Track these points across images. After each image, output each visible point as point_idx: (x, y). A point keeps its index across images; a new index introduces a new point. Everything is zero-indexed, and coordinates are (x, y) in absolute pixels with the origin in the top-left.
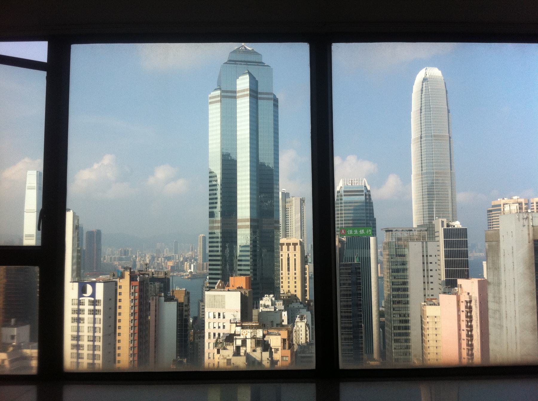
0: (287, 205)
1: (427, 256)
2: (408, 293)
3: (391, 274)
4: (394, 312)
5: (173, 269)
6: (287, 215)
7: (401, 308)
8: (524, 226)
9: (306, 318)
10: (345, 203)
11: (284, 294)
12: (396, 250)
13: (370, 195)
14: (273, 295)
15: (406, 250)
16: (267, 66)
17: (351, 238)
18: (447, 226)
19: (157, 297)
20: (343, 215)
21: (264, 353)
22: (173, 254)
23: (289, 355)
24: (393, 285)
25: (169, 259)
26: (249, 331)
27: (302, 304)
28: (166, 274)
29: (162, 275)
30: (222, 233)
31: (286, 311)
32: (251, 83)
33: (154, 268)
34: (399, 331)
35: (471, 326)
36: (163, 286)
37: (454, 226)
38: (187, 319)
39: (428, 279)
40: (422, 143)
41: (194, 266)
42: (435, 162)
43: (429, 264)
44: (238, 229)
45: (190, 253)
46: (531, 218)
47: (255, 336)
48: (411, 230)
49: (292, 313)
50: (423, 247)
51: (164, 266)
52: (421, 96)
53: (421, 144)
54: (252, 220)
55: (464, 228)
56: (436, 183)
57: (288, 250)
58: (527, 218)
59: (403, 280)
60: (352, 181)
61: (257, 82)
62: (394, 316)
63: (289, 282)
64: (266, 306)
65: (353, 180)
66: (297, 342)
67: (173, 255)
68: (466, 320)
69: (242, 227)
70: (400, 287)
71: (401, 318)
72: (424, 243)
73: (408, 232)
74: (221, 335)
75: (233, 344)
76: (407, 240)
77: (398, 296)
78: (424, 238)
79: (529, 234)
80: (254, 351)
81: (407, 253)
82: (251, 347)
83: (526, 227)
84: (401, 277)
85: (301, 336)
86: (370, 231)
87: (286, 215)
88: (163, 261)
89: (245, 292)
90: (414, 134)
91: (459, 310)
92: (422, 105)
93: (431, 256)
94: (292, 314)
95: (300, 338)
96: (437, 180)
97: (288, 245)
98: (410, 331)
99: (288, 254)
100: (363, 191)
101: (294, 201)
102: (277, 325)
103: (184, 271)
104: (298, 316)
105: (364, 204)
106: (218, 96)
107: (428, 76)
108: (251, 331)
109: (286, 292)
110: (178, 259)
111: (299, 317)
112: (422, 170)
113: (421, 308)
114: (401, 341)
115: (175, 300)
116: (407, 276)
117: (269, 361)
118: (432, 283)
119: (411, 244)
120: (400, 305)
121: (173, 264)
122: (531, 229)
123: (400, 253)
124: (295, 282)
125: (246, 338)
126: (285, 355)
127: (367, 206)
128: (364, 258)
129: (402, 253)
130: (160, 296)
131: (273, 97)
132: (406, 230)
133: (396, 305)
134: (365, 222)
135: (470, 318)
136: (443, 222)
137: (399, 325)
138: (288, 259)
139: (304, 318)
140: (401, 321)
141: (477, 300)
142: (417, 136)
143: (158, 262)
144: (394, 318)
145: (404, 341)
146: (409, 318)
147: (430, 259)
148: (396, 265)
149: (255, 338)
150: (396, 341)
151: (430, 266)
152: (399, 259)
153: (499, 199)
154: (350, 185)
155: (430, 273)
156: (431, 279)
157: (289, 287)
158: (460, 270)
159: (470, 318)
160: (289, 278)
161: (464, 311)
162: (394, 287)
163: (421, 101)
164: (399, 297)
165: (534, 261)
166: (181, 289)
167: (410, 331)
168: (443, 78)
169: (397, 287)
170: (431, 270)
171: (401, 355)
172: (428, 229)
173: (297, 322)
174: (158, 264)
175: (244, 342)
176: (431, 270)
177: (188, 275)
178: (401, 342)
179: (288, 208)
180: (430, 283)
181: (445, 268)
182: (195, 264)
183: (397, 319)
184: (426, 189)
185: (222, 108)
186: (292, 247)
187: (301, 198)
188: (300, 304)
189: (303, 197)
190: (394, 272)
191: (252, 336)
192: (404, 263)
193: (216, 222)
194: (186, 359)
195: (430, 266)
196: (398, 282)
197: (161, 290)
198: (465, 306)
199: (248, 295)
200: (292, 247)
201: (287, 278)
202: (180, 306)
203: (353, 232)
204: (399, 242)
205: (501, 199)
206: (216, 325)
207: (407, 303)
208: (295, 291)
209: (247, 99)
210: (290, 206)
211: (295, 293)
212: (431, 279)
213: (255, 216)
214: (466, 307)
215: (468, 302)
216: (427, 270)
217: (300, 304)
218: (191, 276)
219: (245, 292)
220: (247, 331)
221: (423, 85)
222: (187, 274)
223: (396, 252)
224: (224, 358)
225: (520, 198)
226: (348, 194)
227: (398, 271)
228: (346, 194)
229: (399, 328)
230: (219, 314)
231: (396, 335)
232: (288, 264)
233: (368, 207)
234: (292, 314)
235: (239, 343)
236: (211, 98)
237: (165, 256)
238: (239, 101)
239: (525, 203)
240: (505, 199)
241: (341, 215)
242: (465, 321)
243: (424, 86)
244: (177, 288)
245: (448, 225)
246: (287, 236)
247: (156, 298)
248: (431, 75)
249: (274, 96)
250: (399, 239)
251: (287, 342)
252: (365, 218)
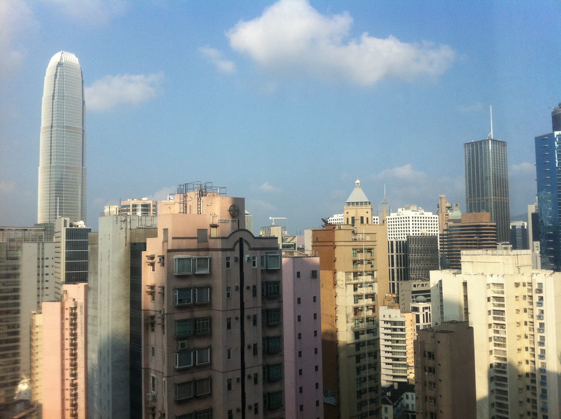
2: (19, 301)
7: (10, 318)
8: (122, 229)
12: (7, 253)
15: (19, 252)
18: (70, 226)
37: (78, 226)
40: (53, 132)
42: (66, 155)
43: (45, 268)
46: (129, 221)
50: (39, 249)
53: (51, 134)
55: (88, 229)
59: (14, 287)
70: (9, 294)
72: (41, 244)
73: (23, 232)
78: (41, 237)
79: (126, 237)
81: (20, 256)
83: (124, 230)
84: (12, 284)
90: (45, 122)
91: (62, 318)
92: (55, 91)
93: (47, 259)
96: (67, 175)
107: (63, 61)
112: (51, 163)
116: (18, 281)
122: (129, 232)
123: (11, 256)
129: (13, 256)
132: (21, 229)
135: (74, 325)
136: (65, 221)
140: (10, 334)
141: (82, 306)
142: (47, 125)
147: (46, 262)
151: (46, 270)
153: (128, 200)
159: (74, 325)
163: (54, 87)
165: (130, 265)
168: (79, 66)
170: (47, 274)
176: (47, 274)
192: (17, 267)
195: (46, 270)
196: (8, 289)
207: (18, 312)
214: (71, 314)
221: (57, 69)
223: (7, 255)
225: (149, 199)
240: (135, 199)
243: (59, 71)
245: (71, 225)
248: (67, 60)
250: (11, 240)
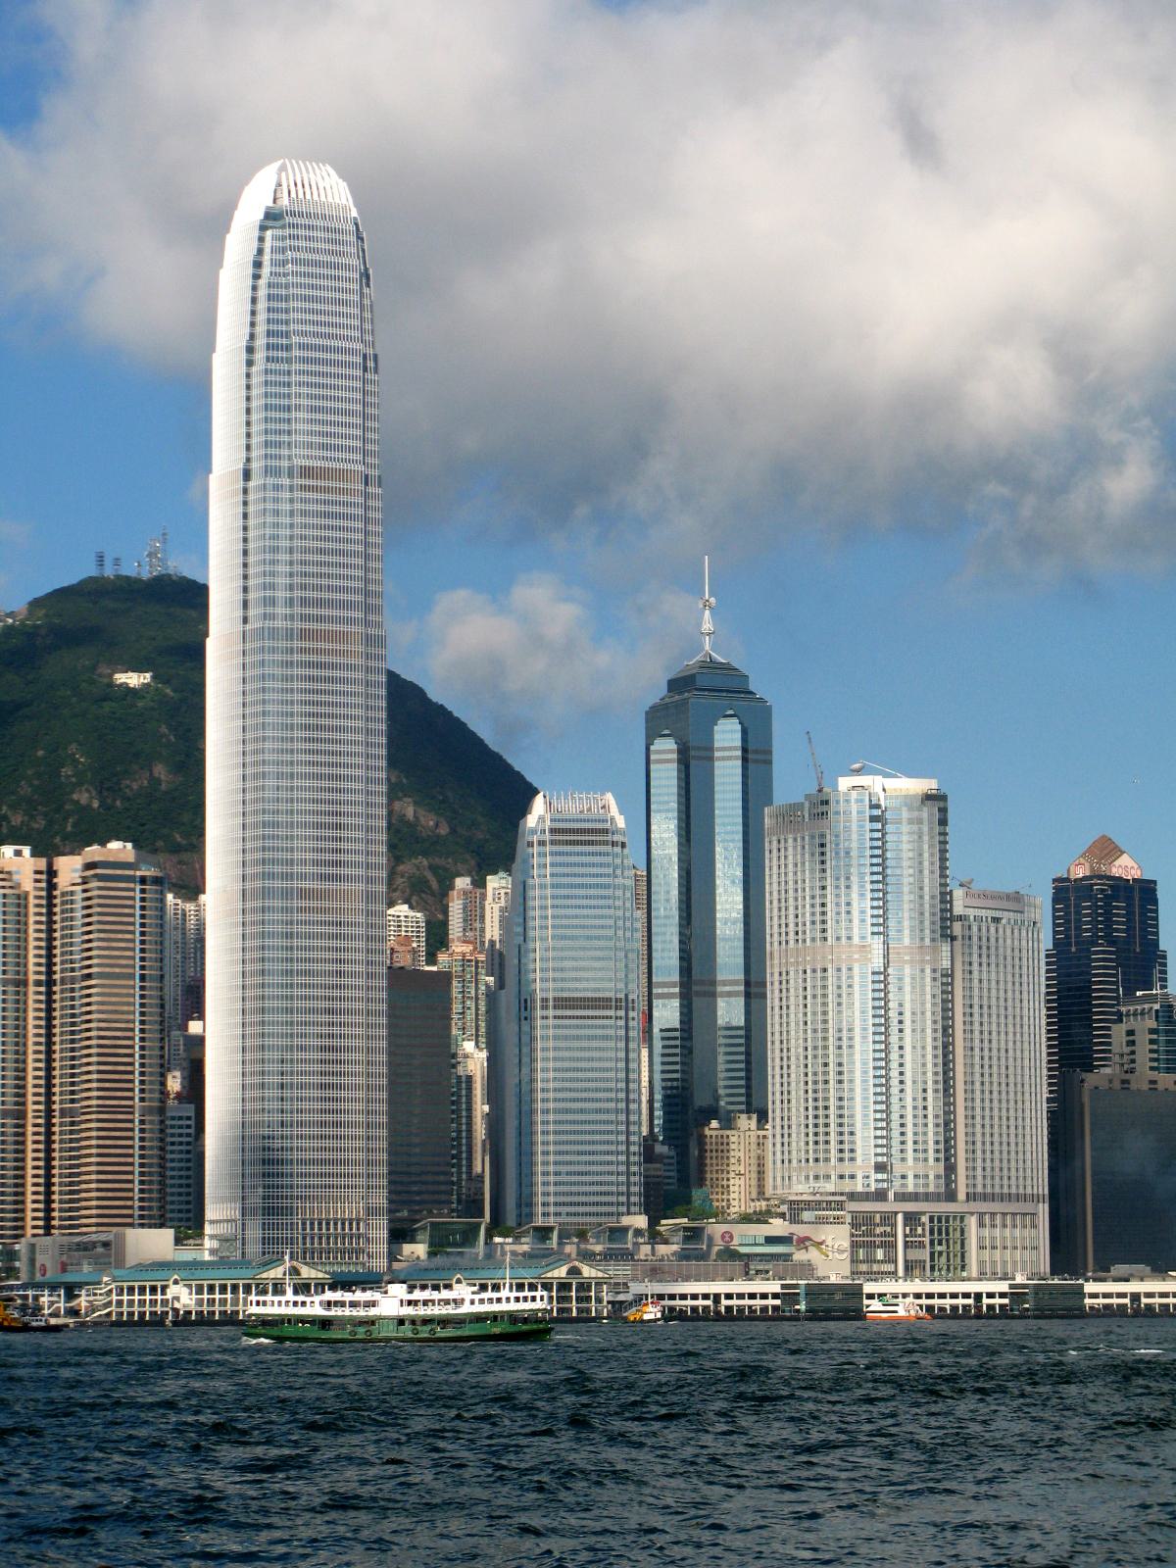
112: (245, 620)
221: (261, 239)
241: (543, 892)
243: (268, 245)
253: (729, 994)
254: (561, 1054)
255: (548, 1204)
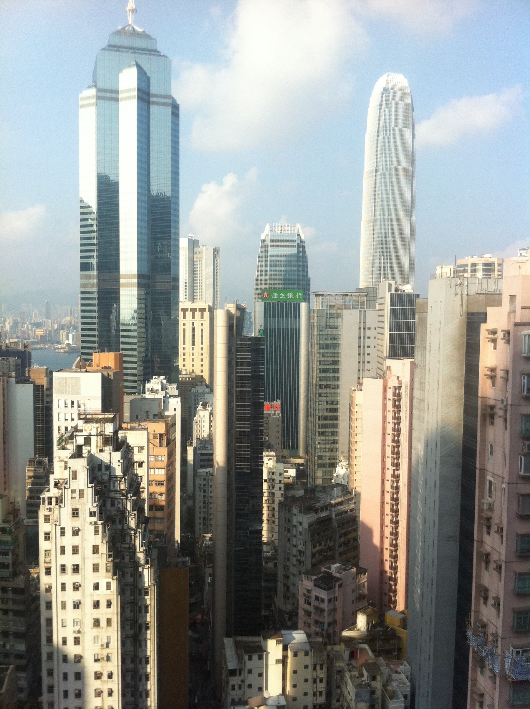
0: (196, 256)
1: (364, 328)
2: (339, 375)
3: (318, 351)
4: (320, 398)
5: (43, 340)
6: (195, 271)
9: (211, 406)
10: (271, 256)
11: (186, 374)
12: (326, 321)
13: (304, 247)
14: (164, 377)
15: (340, 320)
16: (164, 56)
17: (275, 303)
19: (5, 378)
20: (268, 273)
21: (114, 454)
22: (45, 320)
23: (166, 455)
24: (320, 364)
25: (38, 325)
26: (94, 425)
27: (208, 388)
28: (25, 347)
29: (20, 348)
30: (99, 292)
31: (180, 398)
32: (139, 79)
33: (17, 337)
34: (325, 422)
35: (399, 418)
36: (20, 363)
37: (404, 291)
38: (49, 406)
39: (364, 358)
41: (73, 336)
44: (121, 289)
45: (68, 318)
47: (102, 431)
48: (347, 295)
49: (195, 400)
50: (360, 317)
51: (31, 334)
52: (380, 112)
53: (375, 180)
54: (140, 276)
55: (416, 294)
56: (391, 233)
57: (193, 317)
58: (461, 284)
59: (333, 359)
60: (281, 226)
61: (148, 79)
62: (320, 403)
63: (193, 360)
64: (153, 391)
65: (283, 225)
66: (199, 435)
67: (44, 321)
68: (393, 411)
69: (127, 285)
70: (328, 367)
71: (328, 407)
72: (363, 311)
74: (69, 428)
75: (72, 443)
76: (340, 308)
77: (326, 379)
78: (362, 304)
79: (462, 305)
80: (101, 451)
82: (97, 446)
83: (459, 296)
84: (331, 355)
85: (203, 429)
86: (301, 294)
87: (194, 271)
88: (30, 328)
89: (108, 373)
90: (368, 165)
91: (385, 398)
93: (369, 329)
94: (195, 401)
95: (203, 431)
97: (193, 310)
98: (338, 422)
99: (193, 323)
100: (294, 241)
101: (204, 252)
102: (155, 416)
103: (59, 343)
104: (201, 403)
105: (296, 259)
106: (91, 97)
108: (97, 425)
109: (190, 373)
110: (51, 326)
111: (202, 405)
112: (375, 216)
113: (350, 394)
114: (327, 434)
115: (31, 381)
116: (338, 353)
117: (120, 464)
118: (368, 362)
119: (346, 314)
120: (328, 390)
121: (44, 334)
124: (202, 360)
125: (90, 435)
126: (161, 454)
127: (300, 261)
128: (291, 329)
129: (333, 324)
130: (11, 377)
131: (171, 102)
132: (342, 295)
133: (323, 390)
134: (296, 282)
135: (397, 407)
136: (390, 285)
137: (325, 414)
138: (193, 330)
139: (209, 406)
140: (328, 410)
141: (407, 386)
143: (23, 329)
144: (320, 406)
145: (330, 434)
146: (338, 406)
147: (368, 333)
148: (326, 339)
149: (102, 435)
150: (321, 434)
151: (368, 342)
152: (330, 332)
153: (466, 258)
154: (279, 232)
155: (368, 351)
156: (367, 358)
157: (193, 365)
158: (401, 346)
159: (397, 407)
160: (193, 354)
161: (392, 399)
162: (321, 367)
163: (379, 120)
164: (327, 381)
166: (40, 368)
167: (338, 422)
169: (326, 367)
170: (369, 347)
171: (326, 452)
172: (368, 293)
173: (199, 410)
174: (23, 332)
175: (88, 440)
176: (369, 347)
177: (65, 348)
178: (327, 436)
179: (197, 262)
180: (366, 362)
181: (390, 344)
182: (74, 333)
183: (323, 407)
184: (378, 241)
185: (99, 115)
186: (198, 314)
187: (215, 248)
188: (206, 388)
189: (217, 246)
190: (323, 349)
191: (98, 433)
192: (336, 337)
193: (90, 277)
194: (47, 459)
195: (368, 342)
197: (18, 368)
198: (393, 393)
199: (112, 377)
200: (198, 314)
201: (200, 354)
202: (38, 389)
203: (279, 296)
204: (331, 311)
205: (470, 257)
206: (69, 417)
207: (337, 387)
208: (202, 371)
209: (134, 103)
210: (200, 258)
211: (201, 374)
212: (367, 358)
213: (146, 271)
214: (394, 394)
215: (397, 388)
216: (364, 347)
217: (206, 388)
218: (68, 349)
219: (108, 373)
220: (91, 426)
221: (382, 97)
222: (63, 346)
223: (326, 323)
224: (60, 460)
226: (283, 244)
227: (328, 347)
228: (273, 244)
229: (325, 418)
230: (73, 403)
231: (320, 426)
232: (193, 336)
233: (301, 264)
234: (195, 401)
235: (80, 441)
236: (82, 99)
237: (32, 322)
238: (121, 104)
239: (498, 264)
242: (391, 411)
243: (384, 99)
244: (35, 366)
245: (397, 290)
246: (195, 299)
247: (3, 379)
249: (174, 100)
250: (331, 307)
251: (165, 438)
252: (296, 277)
253: (127, 98)
254: (393, 258)
255: (267, 275)
